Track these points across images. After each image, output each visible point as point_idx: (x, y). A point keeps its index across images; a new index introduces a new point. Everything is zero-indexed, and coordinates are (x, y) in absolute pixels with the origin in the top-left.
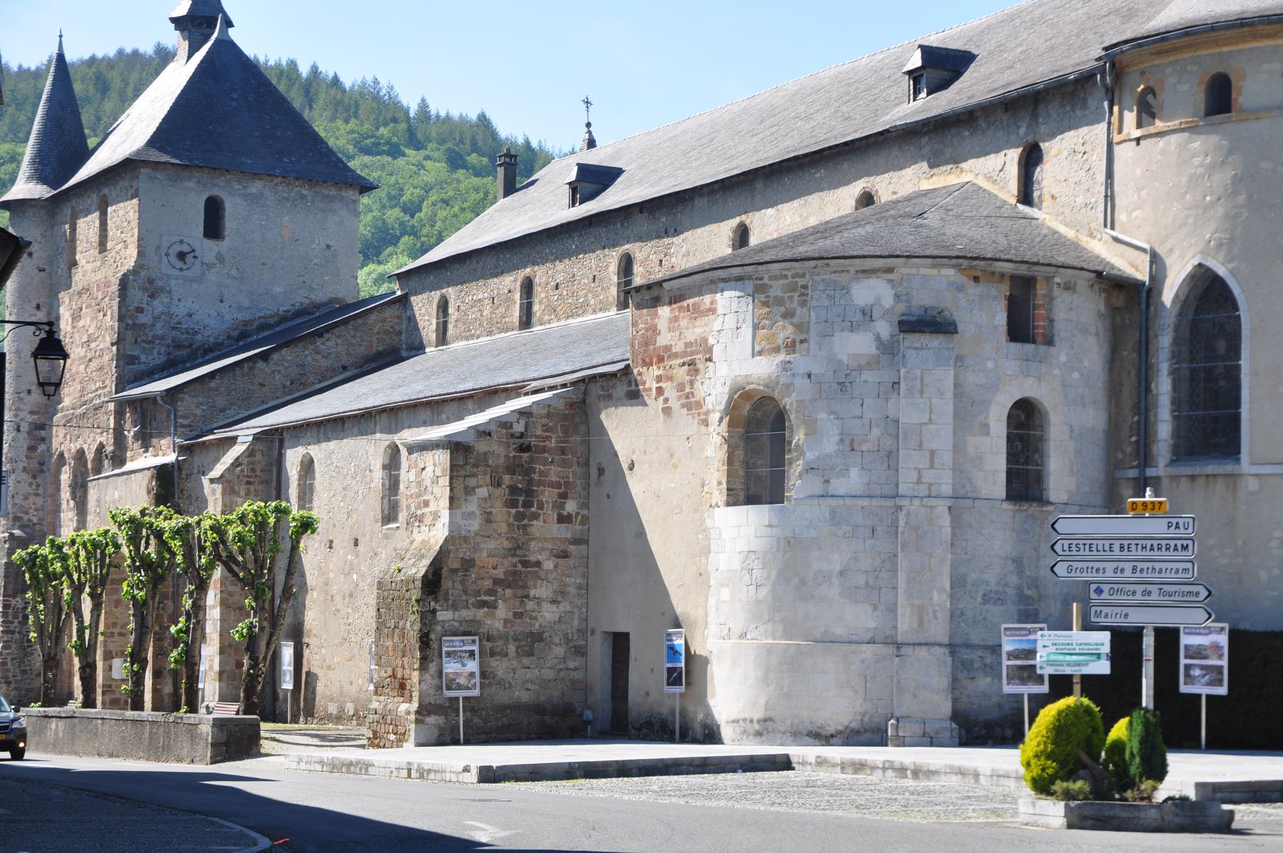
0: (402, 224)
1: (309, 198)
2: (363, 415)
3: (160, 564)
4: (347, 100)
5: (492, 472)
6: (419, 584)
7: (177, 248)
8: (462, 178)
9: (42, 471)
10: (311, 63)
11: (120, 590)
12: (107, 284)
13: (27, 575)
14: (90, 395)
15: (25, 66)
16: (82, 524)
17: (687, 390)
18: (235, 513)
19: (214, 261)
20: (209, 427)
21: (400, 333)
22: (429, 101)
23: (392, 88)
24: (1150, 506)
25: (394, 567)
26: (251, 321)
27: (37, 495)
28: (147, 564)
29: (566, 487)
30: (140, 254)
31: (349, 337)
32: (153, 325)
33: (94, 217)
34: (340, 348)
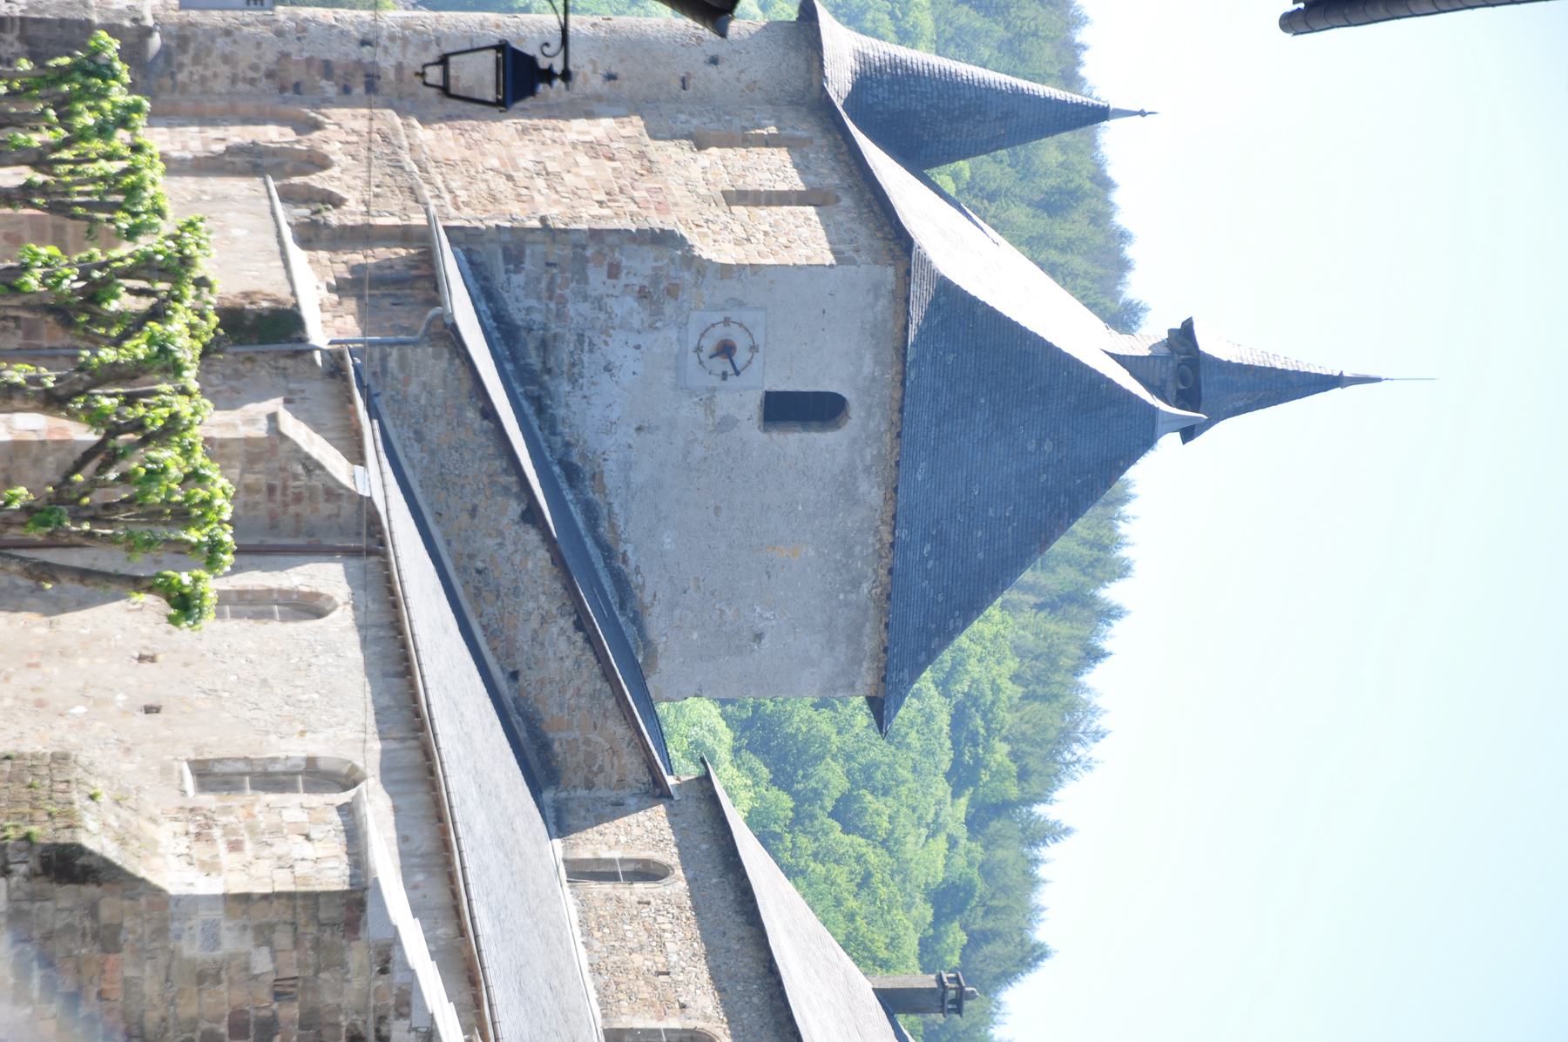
0: (817, 795)
1: (853, 597)
2: (417, 714)
3: (96, 319)
4: (1057, 677)
5: (305, 980)
6: (65, 837)
7: (741, 341)
8: (914, 912)
9: (282, 89)
10: (1127, 606)
11: (41, 241)
12: (662, 208)
13: (65, 61)
14: (439, 180)
15: (1085, 57)
16: (176, 167)
18: (207, 461)
19: (720, 413)
20: (383, 409)
21: (589, 785)
22: (1065, 844)
23: (1088, 767)
25: (99, 785)
26: (602, 489)
27: (234, 80)
28: (95, 293)
30: (726, 270)
31: (577, 682)
32: (585, 298)
33: (793, 181)
34: (553, 665)
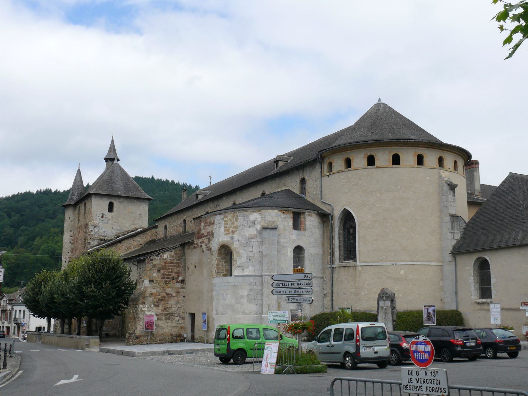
17: (208, 245)
24: (299, 271)
29: (179, 273)
32: (95, 234)
